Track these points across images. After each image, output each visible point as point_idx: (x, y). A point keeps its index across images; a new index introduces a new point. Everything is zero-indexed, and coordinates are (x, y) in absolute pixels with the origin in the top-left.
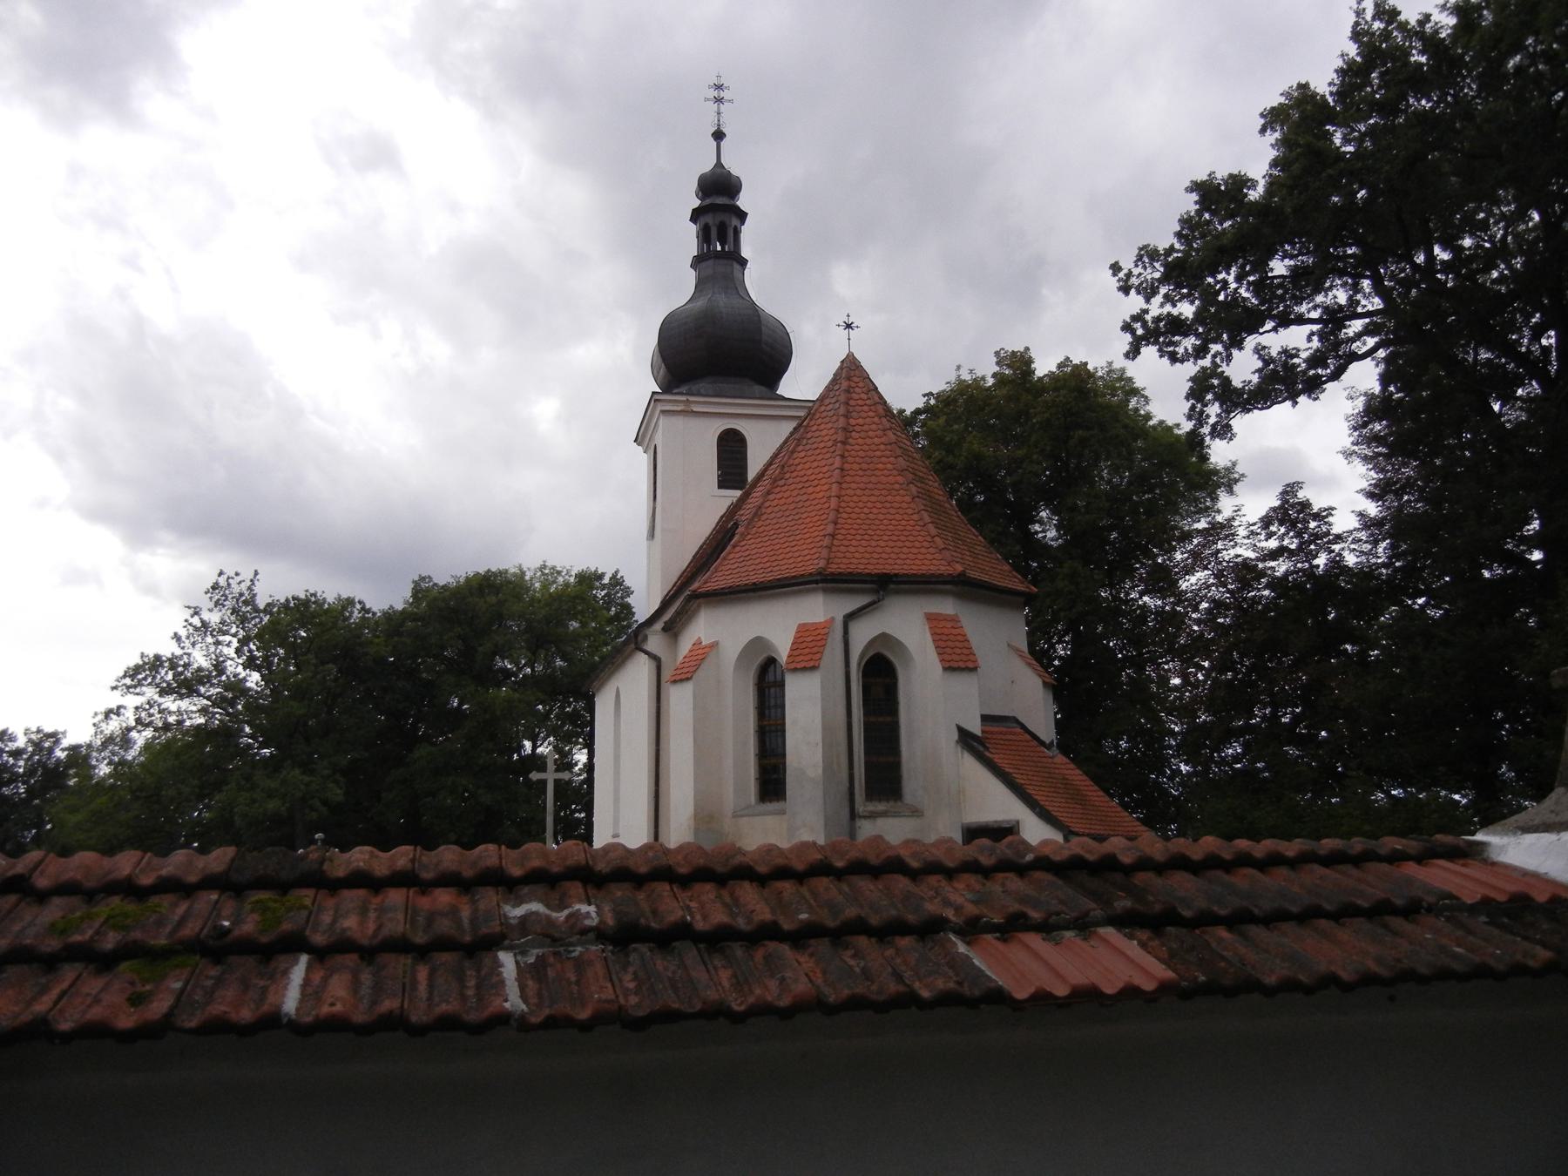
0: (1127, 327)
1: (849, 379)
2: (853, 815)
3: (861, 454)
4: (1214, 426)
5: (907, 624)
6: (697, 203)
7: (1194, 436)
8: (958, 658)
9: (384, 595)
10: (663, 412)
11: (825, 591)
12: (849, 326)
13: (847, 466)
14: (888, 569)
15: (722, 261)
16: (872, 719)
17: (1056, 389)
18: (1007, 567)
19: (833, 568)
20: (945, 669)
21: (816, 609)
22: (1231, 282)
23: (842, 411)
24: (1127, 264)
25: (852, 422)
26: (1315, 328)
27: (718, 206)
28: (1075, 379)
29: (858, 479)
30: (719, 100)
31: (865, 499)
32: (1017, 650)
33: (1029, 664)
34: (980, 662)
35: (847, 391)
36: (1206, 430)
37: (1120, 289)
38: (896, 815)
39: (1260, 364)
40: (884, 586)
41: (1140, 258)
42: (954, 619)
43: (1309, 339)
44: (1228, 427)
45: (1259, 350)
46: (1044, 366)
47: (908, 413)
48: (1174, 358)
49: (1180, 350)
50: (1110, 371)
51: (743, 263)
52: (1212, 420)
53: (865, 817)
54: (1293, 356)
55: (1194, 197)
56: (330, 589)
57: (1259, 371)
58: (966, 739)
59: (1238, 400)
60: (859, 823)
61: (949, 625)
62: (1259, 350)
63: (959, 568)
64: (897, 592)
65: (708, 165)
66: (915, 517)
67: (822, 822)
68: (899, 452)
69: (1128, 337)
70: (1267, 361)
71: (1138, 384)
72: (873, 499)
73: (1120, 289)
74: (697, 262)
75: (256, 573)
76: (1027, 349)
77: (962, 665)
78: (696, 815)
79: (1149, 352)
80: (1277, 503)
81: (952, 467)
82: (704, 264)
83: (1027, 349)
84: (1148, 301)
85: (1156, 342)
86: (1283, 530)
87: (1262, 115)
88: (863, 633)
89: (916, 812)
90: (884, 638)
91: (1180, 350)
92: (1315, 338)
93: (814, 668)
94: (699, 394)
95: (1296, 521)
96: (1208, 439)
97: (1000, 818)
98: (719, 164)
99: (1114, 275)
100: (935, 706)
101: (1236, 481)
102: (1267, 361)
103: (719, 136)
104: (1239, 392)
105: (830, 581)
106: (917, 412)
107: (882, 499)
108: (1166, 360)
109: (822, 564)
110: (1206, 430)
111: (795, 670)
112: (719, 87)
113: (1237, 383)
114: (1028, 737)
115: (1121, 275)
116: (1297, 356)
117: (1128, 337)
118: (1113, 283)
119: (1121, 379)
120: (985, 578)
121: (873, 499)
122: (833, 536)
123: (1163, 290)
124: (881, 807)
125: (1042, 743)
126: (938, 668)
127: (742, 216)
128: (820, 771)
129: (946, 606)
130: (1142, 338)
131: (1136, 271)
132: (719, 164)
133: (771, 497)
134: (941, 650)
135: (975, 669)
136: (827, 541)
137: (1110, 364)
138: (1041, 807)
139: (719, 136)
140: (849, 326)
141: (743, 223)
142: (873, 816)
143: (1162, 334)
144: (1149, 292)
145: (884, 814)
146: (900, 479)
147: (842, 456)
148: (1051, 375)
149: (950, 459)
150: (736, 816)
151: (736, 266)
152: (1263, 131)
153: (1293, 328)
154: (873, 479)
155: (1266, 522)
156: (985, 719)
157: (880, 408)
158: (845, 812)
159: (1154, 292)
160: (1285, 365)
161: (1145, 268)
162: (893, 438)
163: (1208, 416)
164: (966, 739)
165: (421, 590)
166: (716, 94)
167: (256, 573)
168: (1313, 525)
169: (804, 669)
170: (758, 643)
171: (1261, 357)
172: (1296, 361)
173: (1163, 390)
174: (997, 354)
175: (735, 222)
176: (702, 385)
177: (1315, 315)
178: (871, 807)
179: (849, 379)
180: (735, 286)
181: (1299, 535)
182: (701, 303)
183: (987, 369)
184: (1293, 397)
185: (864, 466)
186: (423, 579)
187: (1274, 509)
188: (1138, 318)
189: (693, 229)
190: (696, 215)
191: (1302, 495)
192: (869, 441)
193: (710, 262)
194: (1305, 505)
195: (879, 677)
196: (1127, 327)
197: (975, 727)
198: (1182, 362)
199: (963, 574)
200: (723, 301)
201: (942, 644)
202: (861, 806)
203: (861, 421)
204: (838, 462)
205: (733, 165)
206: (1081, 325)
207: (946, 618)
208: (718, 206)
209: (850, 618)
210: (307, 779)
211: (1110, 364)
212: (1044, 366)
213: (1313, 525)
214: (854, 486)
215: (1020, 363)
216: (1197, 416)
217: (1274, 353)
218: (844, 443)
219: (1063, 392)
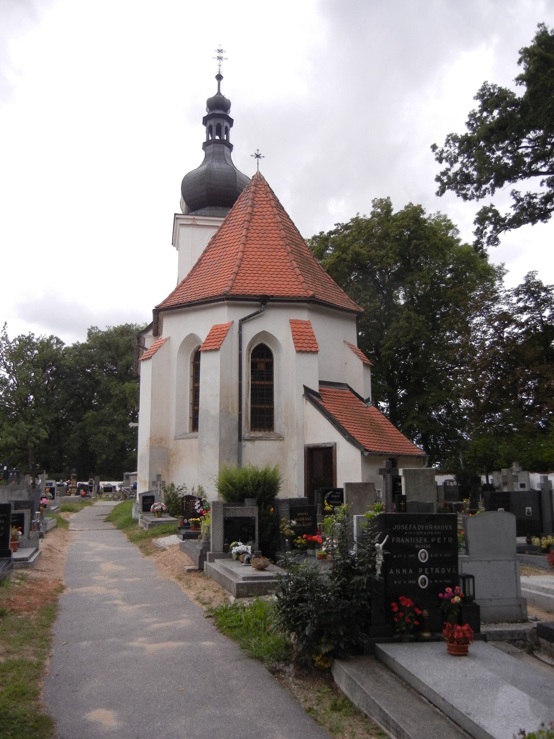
0: (438, 179)
1: (256, 186)
2: (240, 439)
3: (260, 228)
4: (489, 238)
5: (278, 326)
6: (206, 114)
7: (478, 245)
8: (306, 345)
9: (72, 338)
10: (181, 224)
11: (229, 305)
12: (258, 156)
13: (249, 235)
14: (268, 293)
15: (218, 145)
16: (257, 383)
17: (403, 219)
18: (347, 297)
19: (234, 292)
20: (298, 352)
21: (224, 316)
22: (500, 155)
23: (250, 203)
24: (441, 145)
25: (255, 210)
26: (545, 177)
27: (218, 115)
28: (414, 214)
29: (255, 242)
30: (220, 58)
31: (259, 253)
32: (351, 346)
33: (356, 353)
34: (320, 348)
35: (254, 193)
36: (485, 240)
37: (437, 159)
38: (267, 439)
39: (514, 202)
40: (264, 302)
41: (448, 141)
42: (308, 324)
43: (541, 184)
44: (496, 239)
45: (514, 194)
46: (397, 208)
47: (326, 233)
48: (465, 197)
49: (469, 193)
50: (438, 217)
51: (230, 147)
52: (488, 235)
53: (248, 440)
54: (532, 198)
55: (479, 102)
56: (40, 333)
57: (514, 206)
58: (308, 393)
59: (501, 224)
60: (244, 443)
61: (303, 326)
62: (514, 194)
63: (311, 293)
64: (274, 307)
65: (213, 93)
66: (288, 264)
67: (218, 442)
68: (282, 227)
69: (439, 184)
70: (519, 200)
71: (454, 222)
72: (264, 253)
73: (437, 159)
74: (206, 145)
75: (6, 323)
76: (389, 198)
77: (308, 349)
78: (151, 439)
79: (450, 193)
80: (524, 282)
81: (344, 260)
82: (208, 148)
83: (389, 198)
84: (452, 165)
85: (456, 188)
86: (526, 297)
87: (520, 53)
88: (251, 331)
89: (280, 438)
90: (264, 334)
91: (469, 193)
92: (545, 184)
93: (217, 350)
94: (201, 215)
95: (534, 292)
96: (485, 245)
97: (325, 442)
98: (219, 93)
99: (433, 151)
100: (292, 375)
101: (504, 274)
102: (519, 200)
103: (219, 77)
104: (504, 220)
105: (232, 299)
106: (331, 233)
107: (269, 253)
108: (461, 198)
109: (227, 289)
110: (485, 240)
111: (206, 351)
112: (220, 51)
113: (502, 215)
114: (353, 395)
115: (437, 151)
116: (536, 198)
117: (439, 184)
118: (433, 156)
119: (444, 220)
120: (328, 300)
121: (264, 253)
122: (237, 274)
123: (460, 159)
124: (259, 434)
125: (361, 399)
126: (293, 350)
127: (231, 121)
128: (218, 411)
129: (303, 316)
130: (446, 184)
131: (445, 149)
132: (219, 93)
133: (207, 254)
134: (296, 341)
135: (316, 352)
136: (232, 277)
137: (439, 212)
138: (349, 434)
139: (219, 77)
140: (258, 156)
141: (231, 125)
142: (252, 439)
143: (458, 183)
144: (453, 160)
145: (260, 439)
146: (281, 243)
147: (248, 229)
148: (401, 213)
149: (344, 256)
150: (176, 439)
151: (226, 148)
152: (520, 62)
153: (532, 178)
154: (266, 242)
155: (517, 292)
156: (321, 383)
157: (273, 203)
158: (236, 437)
159: (456, 161)
160: (529, 203)
161: (451, 147)
162: (280, 220)
163: (486, 233)
164: (308, 393)
165: (93, 335)
166: (218, 55)
167: (6, 323)
168: (543, 294)
169: (211, 350)
170: (192, 338)
171: (515, 197)
172: (535, 200)
173: (461, 216)
174: (373, 201)
175: (226, 124)
176: (203, 211)
177: (544, 169)
178: (253, 434)
179: (256, 186)
180: (227, 159)
181: (536, 299)
182: (205, 166)
183: (366, 212)
184: (534, 222)
185: (260, 235)
186: (93, 328)
187: (522, 286)
188: (444, 174)
189: (204, 129)
190: (206, 120)
191: (537, 278)
192: (264, 221)
193: (212, 146)
194: (539, 285)
195: (262, 358)
196: (438, 179)
197: (315, 388)
198: (470, 199)
199: (313, 297)
200: (216, 165)
201: (297, 337)
202: (246, 432)
203: (260, 210)
204: (244, 232)
205: (226, 93)
206: (415, 183)
207: (302, 323)
208: (218, 115)
209: (243, 321)
210: (29, 426)
211: (439, 212)
212: (397, 208)
213: (543, 294)
214: (253, 246)
215: (384, 205)
216: (479, 233)
217: (522, 196)
218: (249, 221)
219: (407, 220)
